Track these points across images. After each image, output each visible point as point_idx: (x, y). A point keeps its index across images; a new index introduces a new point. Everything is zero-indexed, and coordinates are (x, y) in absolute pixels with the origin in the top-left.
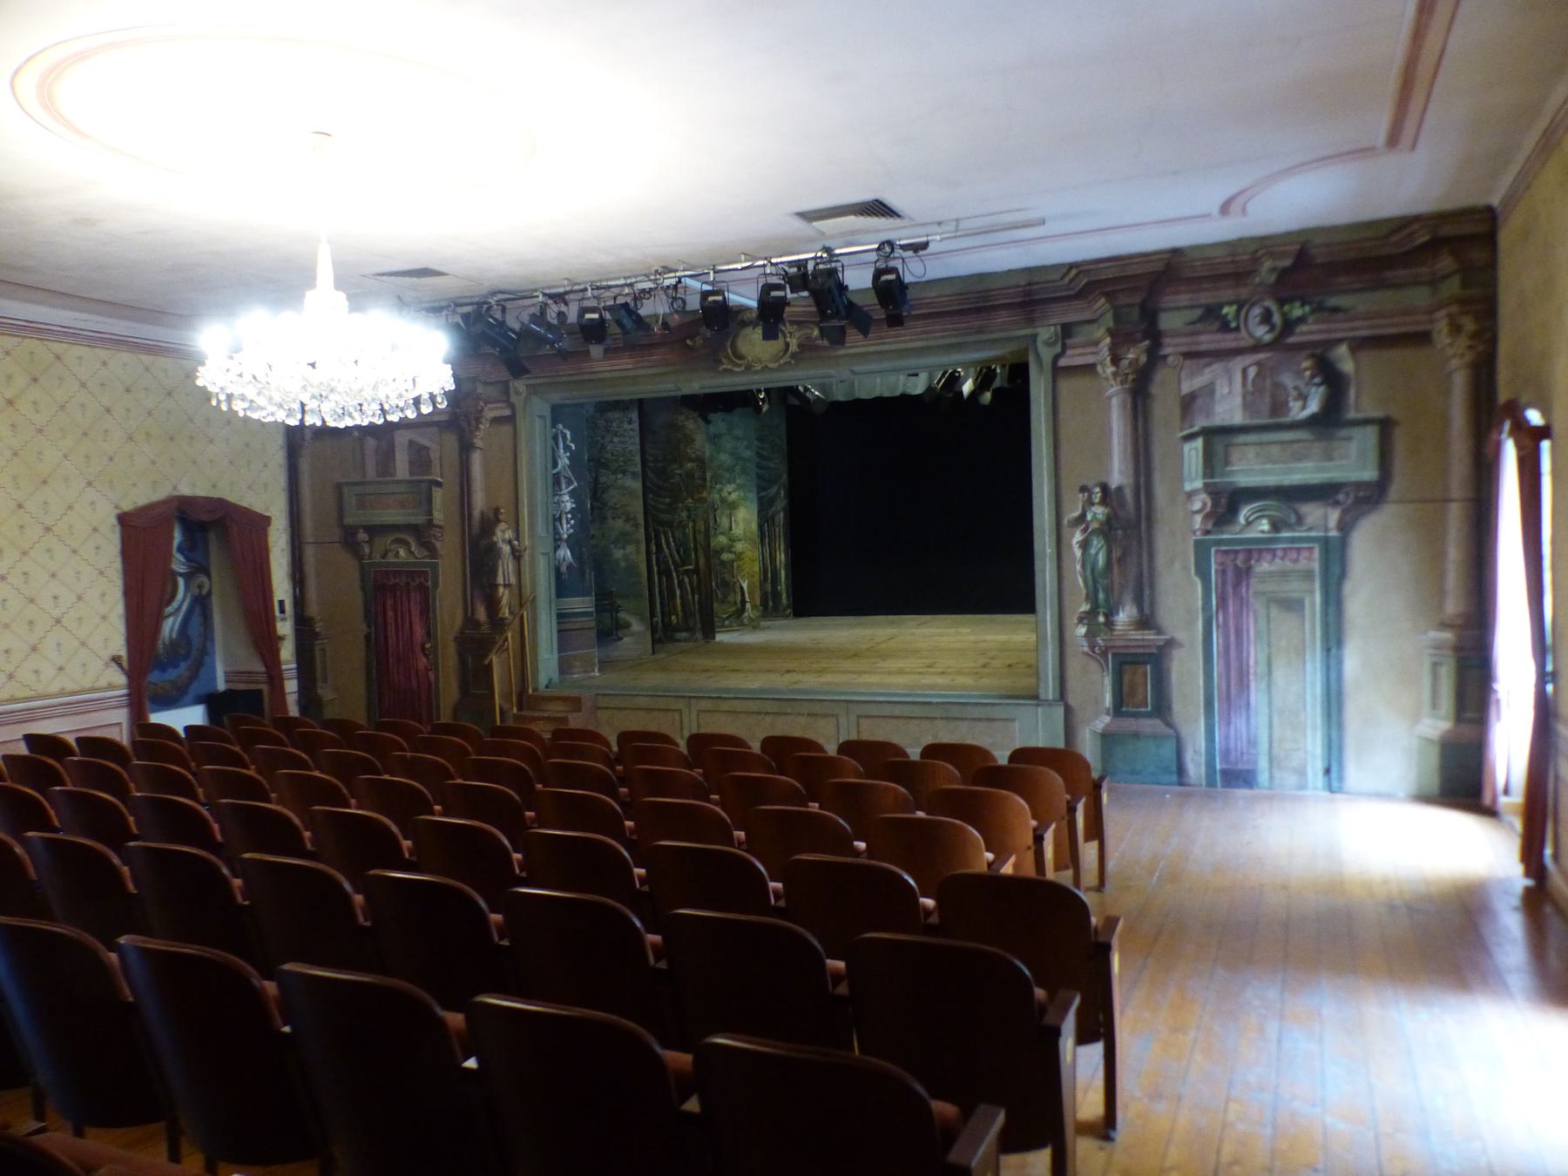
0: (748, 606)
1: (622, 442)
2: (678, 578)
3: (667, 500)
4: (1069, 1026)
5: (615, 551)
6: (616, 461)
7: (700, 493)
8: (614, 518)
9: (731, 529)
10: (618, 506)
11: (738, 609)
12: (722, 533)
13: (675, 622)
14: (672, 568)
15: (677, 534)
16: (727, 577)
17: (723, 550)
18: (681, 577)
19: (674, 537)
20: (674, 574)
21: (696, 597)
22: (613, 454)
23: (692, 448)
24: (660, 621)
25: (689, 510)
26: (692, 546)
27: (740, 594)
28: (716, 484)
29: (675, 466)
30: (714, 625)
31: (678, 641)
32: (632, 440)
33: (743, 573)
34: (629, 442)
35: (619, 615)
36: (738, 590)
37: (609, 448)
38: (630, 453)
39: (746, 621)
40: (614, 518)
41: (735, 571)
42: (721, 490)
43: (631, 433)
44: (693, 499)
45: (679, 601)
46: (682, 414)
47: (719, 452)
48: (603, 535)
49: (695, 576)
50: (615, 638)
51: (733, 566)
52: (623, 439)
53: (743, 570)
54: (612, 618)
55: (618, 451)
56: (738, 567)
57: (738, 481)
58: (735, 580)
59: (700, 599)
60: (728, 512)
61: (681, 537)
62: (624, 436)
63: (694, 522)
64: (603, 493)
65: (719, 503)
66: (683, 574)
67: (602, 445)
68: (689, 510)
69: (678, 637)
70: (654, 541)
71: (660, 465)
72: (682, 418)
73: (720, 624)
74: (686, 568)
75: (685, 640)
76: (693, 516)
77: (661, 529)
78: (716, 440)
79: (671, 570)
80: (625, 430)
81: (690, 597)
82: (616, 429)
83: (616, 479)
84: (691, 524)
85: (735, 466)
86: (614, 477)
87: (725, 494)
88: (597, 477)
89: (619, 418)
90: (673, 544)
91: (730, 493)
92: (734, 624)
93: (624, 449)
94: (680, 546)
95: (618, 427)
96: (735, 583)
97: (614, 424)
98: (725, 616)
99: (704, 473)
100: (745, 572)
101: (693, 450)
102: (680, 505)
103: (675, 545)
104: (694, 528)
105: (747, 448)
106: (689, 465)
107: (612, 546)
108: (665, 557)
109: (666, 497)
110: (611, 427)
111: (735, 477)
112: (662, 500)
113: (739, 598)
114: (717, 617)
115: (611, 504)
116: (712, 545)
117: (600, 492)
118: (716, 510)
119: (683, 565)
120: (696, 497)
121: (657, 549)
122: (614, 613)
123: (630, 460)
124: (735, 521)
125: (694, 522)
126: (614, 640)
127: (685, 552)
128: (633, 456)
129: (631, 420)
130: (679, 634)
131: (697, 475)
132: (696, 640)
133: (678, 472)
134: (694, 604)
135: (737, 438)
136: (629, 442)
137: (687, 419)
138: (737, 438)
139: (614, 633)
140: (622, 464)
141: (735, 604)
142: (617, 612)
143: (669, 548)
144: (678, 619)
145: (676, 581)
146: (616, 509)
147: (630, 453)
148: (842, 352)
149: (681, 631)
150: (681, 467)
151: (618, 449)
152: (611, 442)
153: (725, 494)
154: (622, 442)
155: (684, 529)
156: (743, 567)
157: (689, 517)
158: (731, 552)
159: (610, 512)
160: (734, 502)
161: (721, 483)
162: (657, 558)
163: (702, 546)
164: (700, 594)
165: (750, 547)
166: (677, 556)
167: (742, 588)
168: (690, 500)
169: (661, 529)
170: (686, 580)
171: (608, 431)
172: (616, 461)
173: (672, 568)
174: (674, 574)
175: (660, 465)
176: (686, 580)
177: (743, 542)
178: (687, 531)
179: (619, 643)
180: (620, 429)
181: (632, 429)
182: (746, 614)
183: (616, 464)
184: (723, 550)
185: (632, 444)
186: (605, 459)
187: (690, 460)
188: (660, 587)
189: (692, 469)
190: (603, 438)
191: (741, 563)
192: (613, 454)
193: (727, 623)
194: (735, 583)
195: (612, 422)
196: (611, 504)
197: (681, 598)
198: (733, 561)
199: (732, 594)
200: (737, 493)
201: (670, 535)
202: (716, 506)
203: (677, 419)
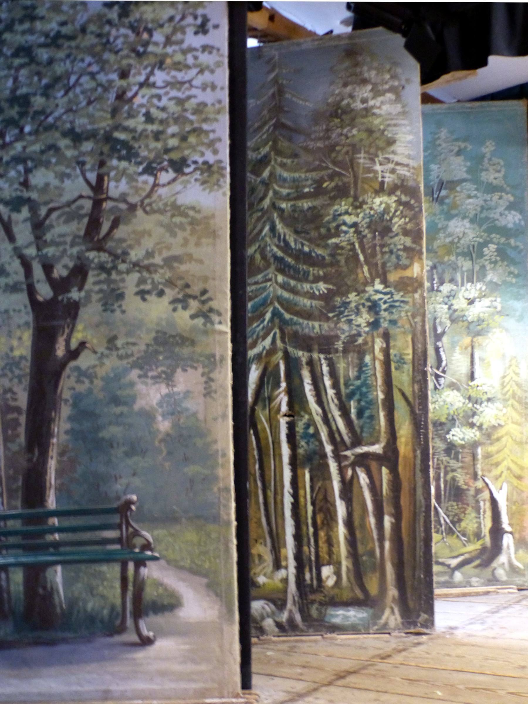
0: (507, 540)
1: (178, 84)
2: (341, 471)
3: (322, 287)
4: (331, 287)
5: (140, 387)
6: (157, 136)
7: (405, 267)
8: (142, 294)
9: (472, 377)
10: (158, 260)
11: (484, 549)
12: (453, 386)
13: (330, 582)
14: (329, 449)
15: (341, 366)
16: (461, 478)
17: (452, 421)
18: (350, 472)
19: (333, 374)
20: (333, 466)
21: (388, 521)
22: (149, 118)
23: (388, 160)
24: (292, 580)
25: (374, 307)
26: (381, 396)
27: (489, 514)
28: (442, 283)
29: (343, 206)
30: (431, 592)
31: (335, 628)
32: (207, 77)
33: (496, 472)
34: (197, 82)
35: (144, 571)
36: (486, 506)
37: (138, 100)
38: (195, 112)
39: (501, 573)
40: (142, 294)
41: (479, 466)
42: (451, 295)
43: (205, 58)
44: (385, 282)
45: (341, 530)
46: (364, 81)
47: (449, 217)
48: (112, 341)
49: (385, 471)
50: (135, 638)
51: (474, 456)
52: (180, 76)
53: (497, 464)
54: (124, 580)
55: (163, 109)
56: (487, 456)
57: (491, 276)
58: (480, 484)
59: (397, 528)
60: (467, 340)
61: (352, 373)
62: (178, 66)
63: (386, 336)
64: (115, 224)
65: (448, 323)
66: (353, 465)
67: (120, 96)
68: (374, 307)
69: (337, 621)
70: (284, 385)
71: (306, 204)
72: (365, 92)
73: (443, 579)
74: (360, 450)
75: (354, 629)
76: (385, 325)
77: (302, 355)
78: (443, 193)
79: (324, 456)
80: (191, 49)
81: (372, 520)
82: (158, 50)
83: (156, 185)
84: (379, 344)
85: (485, 244)
86: (151, 179)
87: (460, 303)
88: (100, 179)
89: (171, 19)
90: (331, 392)
91: (471, 302)
92: (474, 580)
93: (180, 102)
94: (350, 396)
95: (168, 41)
96: (478, 491)
97: (158, 37)
98: (454, 562)
99: (416, 217)
100: (502, 468)
101: (391, 166)
102: (352, 297)
103: (338, 394)
104: (386, 352)
105: (511, 207)
106: (377, 201)
107: (134, 374)
108: (311, 423)
109: (317, 279)
110: (146, 44)
111: (483, 267)
112: (306, 286)
113: (487, 524)
114: (438, 563)
115: (135, 255)
116: (431, 407)
117: (105, 227)
118: (438, 337)
119: (357, 442)
120: (393, 277)
121: (290, 404)
122: (131, 566)
123: (197, 131)
124: (482, 359)
125: (386, 336)
126: (133, 645)
127: (360, 414)
128: (205, 120)
129: (206, 20)
130: (341, 612)
131: (398, 223)
132: (384, 629)
133: (349, 219)
134: (381, 539)
135: (491, 189)
136: (197, 82)
137: (377, 93)
138: (491, 189)
139: (129, 622)
140: (173, 142)
141: (478, 536)
142: (140, 563)
143: (320, 402)
144: (338, 573)
145: (336, 486)
146: (148, 268)
147: (195, 112)
148: (455, 381)
149: (346, 604)
150: (358, 205)
151: (164, 102)
152: (145, 84)
153: (460, 303)
154: (178, 84)
155: (361, 353)
156: (497, 458)
157: (375, 325)
158: (472, 425)
159: (135, 276)
160: (480, 321)
161: (452, 281)
162: (291, 426)
163: (403, 395)
164: (397, 516)
165: (516, 416)
166: (341, 423)
167: (494, 503)
168: (379, 286)
169: (302, 355)
170: (363, 478)
171: (139, 55)
172: (157, 136)
173: (329, 449)
174: (333, 466)
175: (306, 204)
176: (363, 478)
177: (499, 405)
178: (368, 359)
179: (140, 655)
180: (169, 50)
181: (206, 48)
182: (503, 559)
183: (153, 144)
184: (452, 421)
185: (204, 87)
186: (126, 129)
187: (381, 190)
188: (295, 495)
189: (386, 210)
190: (124, 75)
191: (492, 449)
192: (149, 118)
193: (458, 576)
194: (478, 491)
195: (150, 32)
196: (135, 255)
197: (349, 523)
198: (475, 445)
199: (471, 514)
200: (486, 302)
201: (325, 369)
202: (439, 330)
203: (351, 96)
